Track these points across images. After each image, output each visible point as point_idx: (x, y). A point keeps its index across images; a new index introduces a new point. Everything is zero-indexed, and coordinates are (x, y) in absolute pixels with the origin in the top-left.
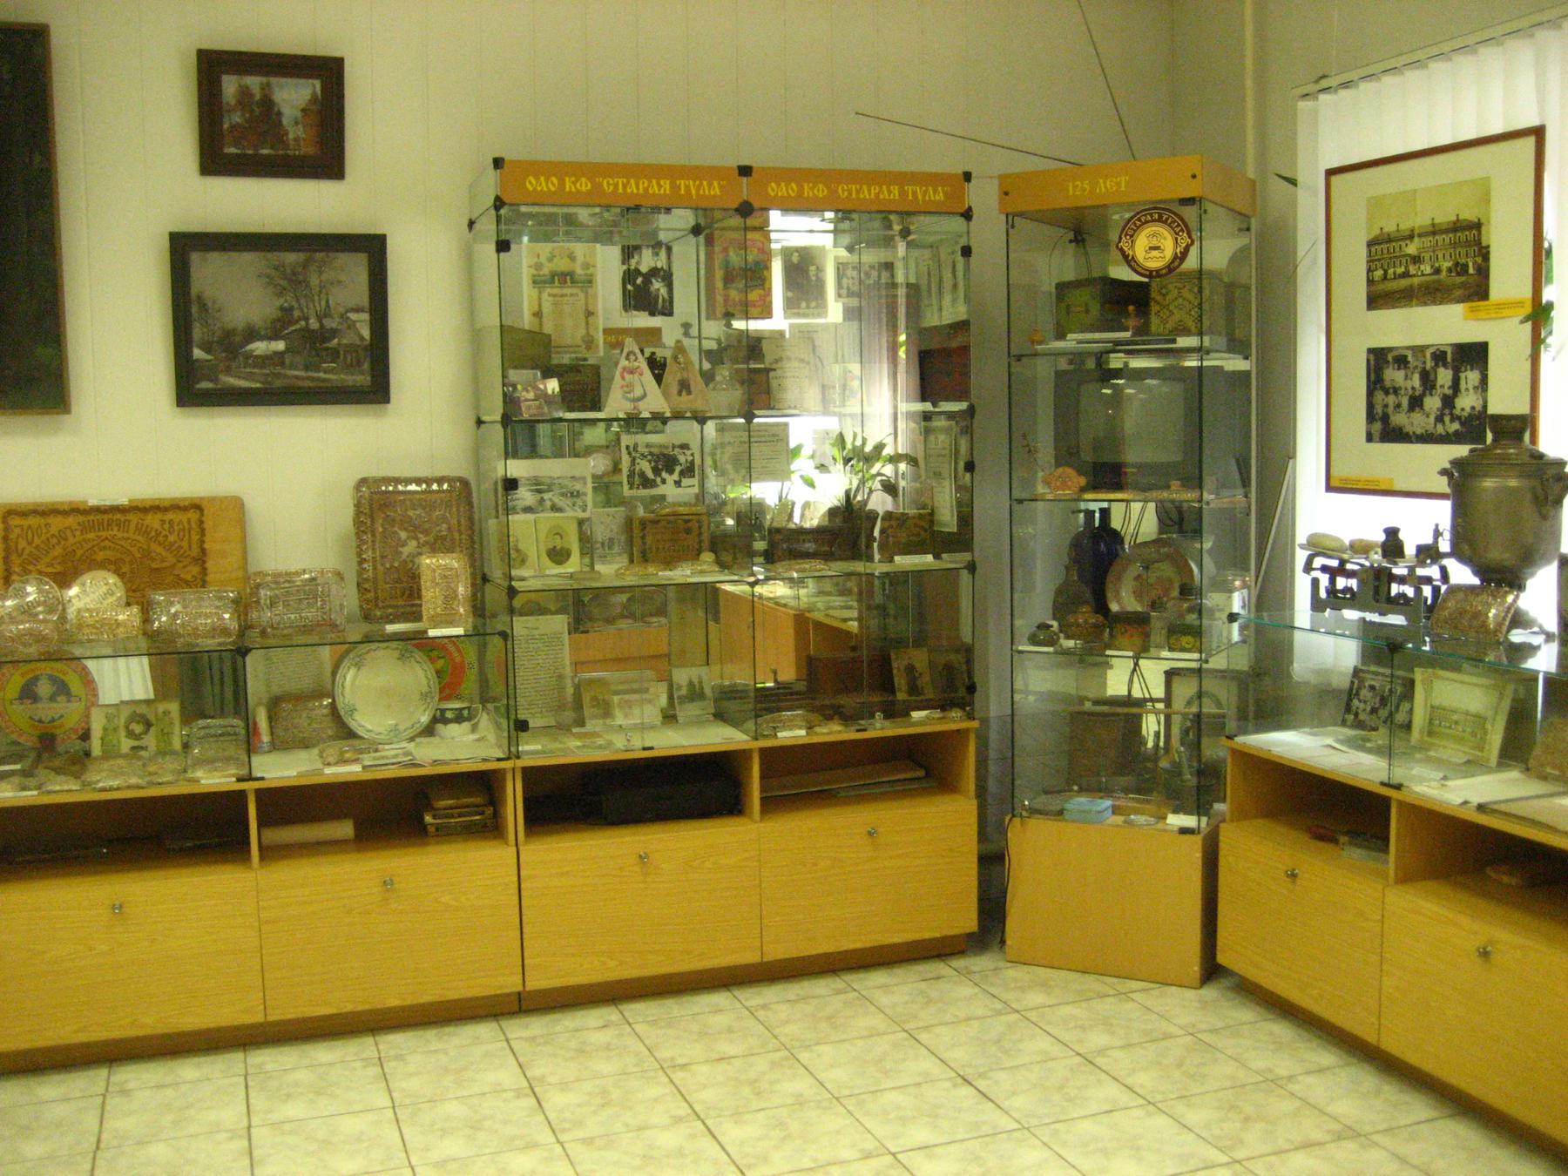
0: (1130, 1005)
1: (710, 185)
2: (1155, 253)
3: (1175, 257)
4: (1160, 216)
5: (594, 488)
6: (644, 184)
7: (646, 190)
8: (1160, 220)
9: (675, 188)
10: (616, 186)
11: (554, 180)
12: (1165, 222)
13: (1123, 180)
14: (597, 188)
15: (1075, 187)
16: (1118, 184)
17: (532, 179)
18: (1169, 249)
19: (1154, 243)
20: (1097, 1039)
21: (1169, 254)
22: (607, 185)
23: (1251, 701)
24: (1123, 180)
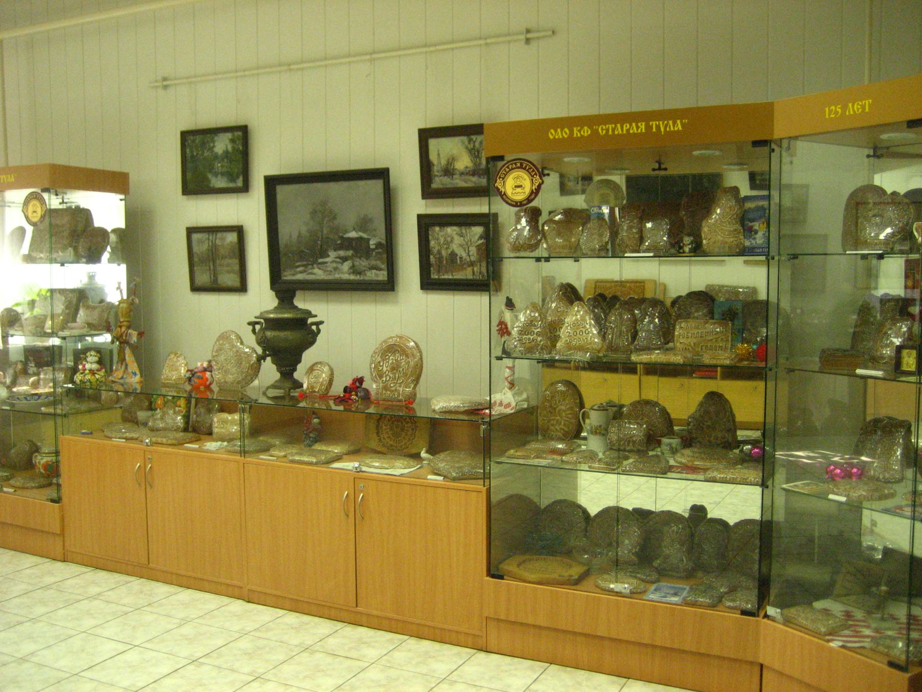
0: (41, 624)
1: (674, 123)
2: (519, 190)
3: (532, 192)
4: (521, 164)
5: (673, 249)
6: (626, 126)
7: (628, 130)
8: (521, 167)
9: (648, 127)
10: (607, 130)
11: (567, 130)
12: (525, 169)
13: (867, 102)
14: (595, 133)
15: (830, 112)
16: (863, 107)
17: (552, 131)
18: (528, 187)
19: (518, 183)
20: (88, 623)
21: (527, 191)
22: (601, 130)
23: (669, 494)
24: (867, 102)
